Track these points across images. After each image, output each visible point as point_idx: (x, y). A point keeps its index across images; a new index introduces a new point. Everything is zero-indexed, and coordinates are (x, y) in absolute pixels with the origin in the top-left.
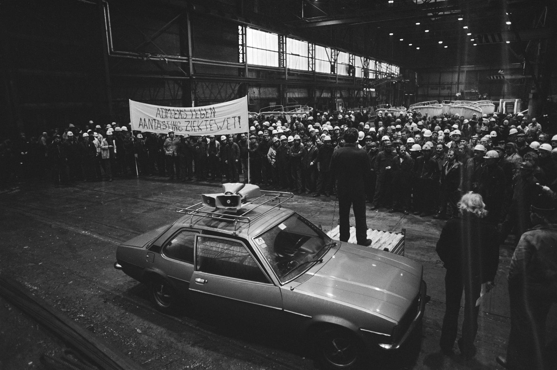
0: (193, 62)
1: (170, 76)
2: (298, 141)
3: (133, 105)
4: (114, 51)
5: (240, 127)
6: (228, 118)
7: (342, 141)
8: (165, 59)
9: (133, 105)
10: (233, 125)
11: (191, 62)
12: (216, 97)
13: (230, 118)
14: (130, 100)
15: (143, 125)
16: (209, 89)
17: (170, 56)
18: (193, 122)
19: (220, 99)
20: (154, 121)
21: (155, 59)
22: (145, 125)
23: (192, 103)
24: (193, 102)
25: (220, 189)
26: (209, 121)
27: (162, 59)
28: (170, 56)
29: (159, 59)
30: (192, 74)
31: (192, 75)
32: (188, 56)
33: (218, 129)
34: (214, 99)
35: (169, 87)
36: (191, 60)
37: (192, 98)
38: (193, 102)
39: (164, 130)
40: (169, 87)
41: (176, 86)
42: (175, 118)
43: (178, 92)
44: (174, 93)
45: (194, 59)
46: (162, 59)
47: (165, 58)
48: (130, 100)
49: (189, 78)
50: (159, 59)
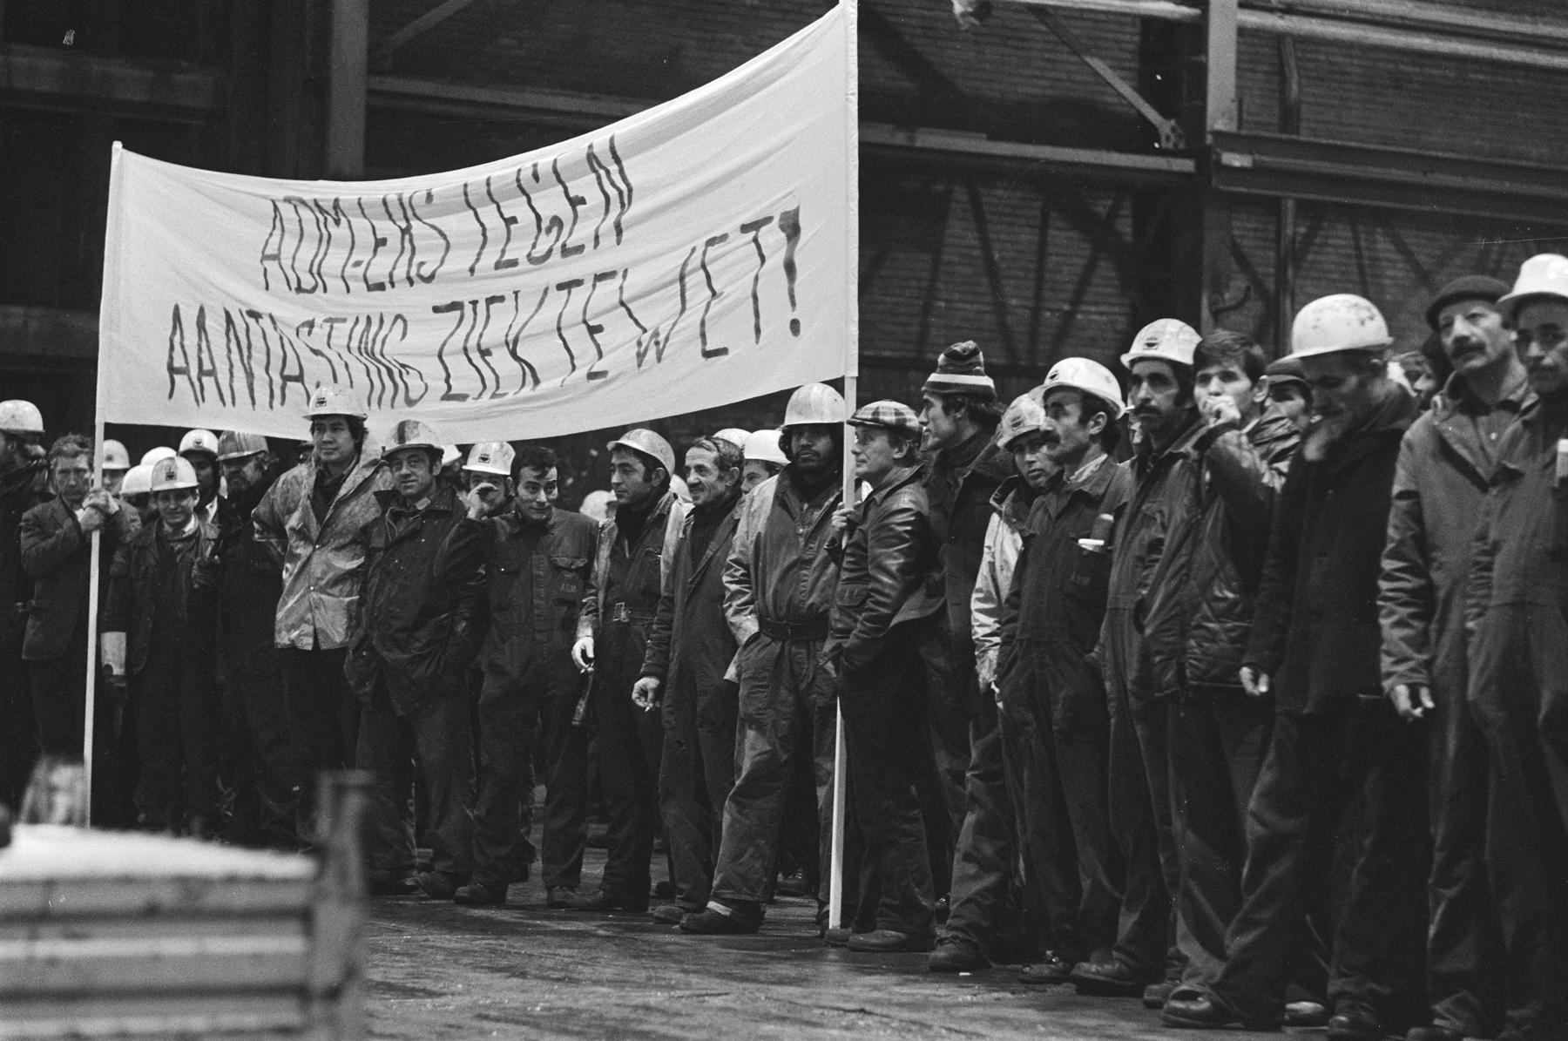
1: (993, 137)
5: (795, 326)
6: (711, 242)
7: (1472, 318)
10: (672, 283)
13: (724, 237)
15: (194, 372)
18: (481, 307)
20: (251, 321)
22: (202, 372)
26: (588, 284)
30: (1220, 125)
31: (1218, 134)
35: (986, 244)
40: (986, 244)
43: (1077, 300)
44: (1036, 312)
49: (1187, 165)
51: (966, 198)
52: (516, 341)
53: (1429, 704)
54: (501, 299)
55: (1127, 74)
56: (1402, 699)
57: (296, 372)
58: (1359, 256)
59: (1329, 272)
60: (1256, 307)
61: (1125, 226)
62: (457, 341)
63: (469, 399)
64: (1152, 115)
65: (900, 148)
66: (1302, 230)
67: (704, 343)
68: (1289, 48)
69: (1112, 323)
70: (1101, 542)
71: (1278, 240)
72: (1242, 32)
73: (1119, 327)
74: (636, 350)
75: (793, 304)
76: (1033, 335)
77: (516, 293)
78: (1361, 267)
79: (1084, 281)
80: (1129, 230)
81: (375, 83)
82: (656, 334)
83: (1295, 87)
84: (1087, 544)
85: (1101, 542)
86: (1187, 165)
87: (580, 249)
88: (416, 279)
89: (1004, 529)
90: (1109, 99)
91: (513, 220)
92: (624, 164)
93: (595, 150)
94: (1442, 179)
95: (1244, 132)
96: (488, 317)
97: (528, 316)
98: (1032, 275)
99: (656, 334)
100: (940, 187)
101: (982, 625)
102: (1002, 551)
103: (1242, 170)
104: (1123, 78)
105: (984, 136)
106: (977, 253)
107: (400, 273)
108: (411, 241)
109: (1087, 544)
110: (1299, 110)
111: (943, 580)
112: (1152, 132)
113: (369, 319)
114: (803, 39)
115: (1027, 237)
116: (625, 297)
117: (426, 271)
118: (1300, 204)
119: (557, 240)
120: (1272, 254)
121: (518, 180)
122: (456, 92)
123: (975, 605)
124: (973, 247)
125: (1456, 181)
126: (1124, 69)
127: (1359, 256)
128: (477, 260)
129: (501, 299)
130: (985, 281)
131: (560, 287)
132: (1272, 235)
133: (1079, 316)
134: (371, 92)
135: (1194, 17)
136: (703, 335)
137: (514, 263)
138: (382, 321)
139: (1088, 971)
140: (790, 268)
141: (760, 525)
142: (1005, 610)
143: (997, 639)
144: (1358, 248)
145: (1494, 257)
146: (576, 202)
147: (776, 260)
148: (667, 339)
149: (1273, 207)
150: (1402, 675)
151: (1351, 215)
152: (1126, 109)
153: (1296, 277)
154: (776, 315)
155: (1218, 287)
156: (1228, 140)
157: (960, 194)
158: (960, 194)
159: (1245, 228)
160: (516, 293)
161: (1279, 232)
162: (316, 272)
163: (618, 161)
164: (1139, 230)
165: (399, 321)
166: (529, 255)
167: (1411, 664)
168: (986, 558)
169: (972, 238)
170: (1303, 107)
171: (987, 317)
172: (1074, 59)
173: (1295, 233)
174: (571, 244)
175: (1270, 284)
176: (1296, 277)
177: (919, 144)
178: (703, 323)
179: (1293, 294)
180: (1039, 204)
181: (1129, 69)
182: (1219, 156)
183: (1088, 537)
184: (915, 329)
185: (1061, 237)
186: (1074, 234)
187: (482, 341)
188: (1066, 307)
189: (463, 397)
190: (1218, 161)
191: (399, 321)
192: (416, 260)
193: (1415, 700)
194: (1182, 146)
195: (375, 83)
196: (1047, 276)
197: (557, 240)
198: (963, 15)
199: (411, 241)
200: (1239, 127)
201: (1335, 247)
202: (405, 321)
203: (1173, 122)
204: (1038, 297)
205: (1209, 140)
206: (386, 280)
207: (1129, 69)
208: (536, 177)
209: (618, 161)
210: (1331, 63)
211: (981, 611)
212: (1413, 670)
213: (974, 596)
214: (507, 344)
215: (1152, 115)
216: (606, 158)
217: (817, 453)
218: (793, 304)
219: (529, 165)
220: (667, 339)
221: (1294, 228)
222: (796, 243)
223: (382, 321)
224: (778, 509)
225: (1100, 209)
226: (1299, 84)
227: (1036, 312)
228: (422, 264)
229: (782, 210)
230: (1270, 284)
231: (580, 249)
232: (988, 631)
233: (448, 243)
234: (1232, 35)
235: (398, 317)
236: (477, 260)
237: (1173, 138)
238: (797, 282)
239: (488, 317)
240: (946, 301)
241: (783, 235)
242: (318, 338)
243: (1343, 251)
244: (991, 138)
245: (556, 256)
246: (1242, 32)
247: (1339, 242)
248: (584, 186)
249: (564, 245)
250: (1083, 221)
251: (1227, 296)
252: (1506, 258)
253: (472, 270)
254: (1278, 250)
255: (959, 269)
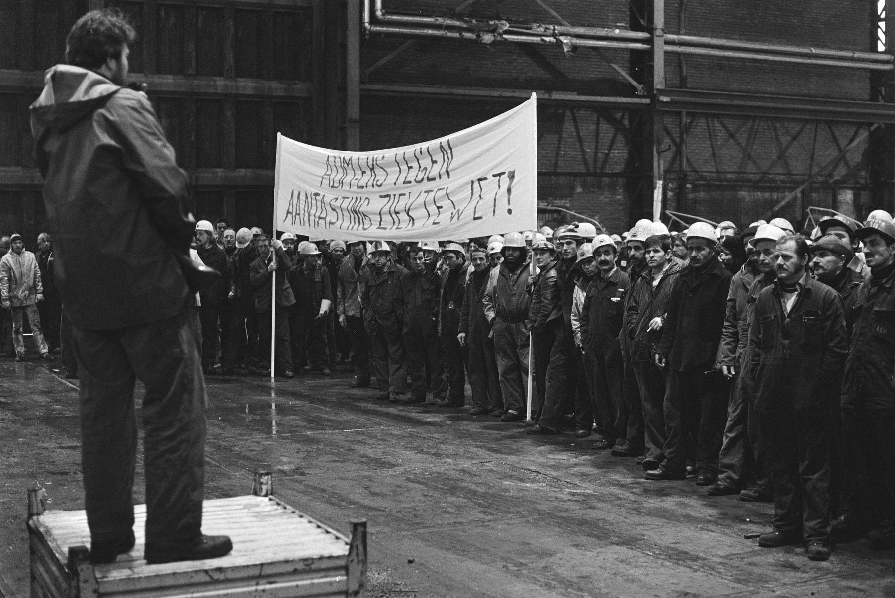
0: (669, 48)
2: (637, 248)
3: (286, 144)
4: (383, 15)
5: (510, 211)
8: (562, 38)
9: (286, 144)
11: (660, 50)
12: (765, 174)
14: (279, 134)
15: (294, 214)
16: (739, 144)
17: (581, 30)
18: (397, 197)
19: (783, 182)
21: (523, 38)
23: (652, 188)
24: (660, 184)
25: (766, 540)
27: (548, 39)
28: (581, 30)
29: (538, 39)
30: (659, 87)
31: (658, 90)
32: (651, 29)
33: (452, 218)
34: (759, 181)
36: (659, 44)
37: (656, 171)
38: (660, 184)
39: (331, 226)
41: (607, 131)
42: (358, 187)
43: (610, 148)
44: (596, 154)
45: (671, 37)
46: (548, 39)
47: (562, 34)
48: (279, 134)
49: (648, 101)
50: (538, 39)
51: (570, 115)
52: (409, 210)
53: (734, 373)
54: (404, 195)
55: (626, 68)
56: (726, 372)
57: (324, 216)
58: (709, 129)
59: (697, 135)
60: (673, 149)
61: (626, 122)
62: (386, 209)
63: (387, 229)
64: (635, 83)
65: (547, 99)
66: (688, 121)
67: (475, 214)
68: (682, 57)
69: (622, 156)
70: (619, 299)
71: (680, 124)
72: (666, 53)
73: (625, 157)
74: (451, 215)
75: (509, 203)
76: (595, 161)
77: (410, 193)
78: (709, 132)
79: (613, 142)
80: (627, 123)
81: (363, 86)
82: (459, 211)
83: (685, 71)
84: (614, 299)
85: (619, 299)
86: (648, 101)
87: (434, 179)
88: (375, 186)
89: (580, 292)
90: (620, 78)
91: (411, 167)
92: (453, 150)
93: (442, 144)
94: (737, 102)
95: (667, 89)
96: (399, 201)
97: (414, 199)
98: (594, 141)
99: (459, 211)
100: (561, 111)
101: (574, 325)
102: (580, 299)
103: (667, 102)
104: (624, 70)
105: (576, 93)
106: (574, 134)
107: (370, 183)
108: (374, 172)
109: (614, 299)
110: (686, 78)
111: (562, 304)
112: (636, 89)
113: (356, 198)
114: (517, 111)
115: (592, 127)
116: (448, 192)
117: (379, 183)
118: (687, 113)
119: (425, 175)
120: (678, 129)
121: (415, 153)
122: (391, 88)
123: (572, 318)
124: (573, 132)
125: (742, 103)
126: (624, 67)
127: (709, 129)
128: (397, 180)
129: (404, 195)
130: (578, 144)
131: (425, 192)
132: (678, 123)
133: (611, 154)
134: (361, 90)
135: (649, 49)
136: (475, 212)
137: (410, 182)
138: (361, 199)
139: (618, 449)
140: (509, 191)
141: (495, 283)
142: (583, 318)
143: (579, 329)
144: (708, 126)
145: (756, 127)
146: (434, 162)
147: (504, 187)
148: (462, 212)
149: (679, 114)
150: (726, 362)
151: (706, 116)
152: (625, 81)
153: (686, 137)
154: (502, 206)
155: (659, 143)
156: (662, 92)
157: (568, 113)
158: (568, 113)
159: (668, 121)
160: (410, 193)
161: (680, 122)
162: (341, 183)
163: (451, 149)
164: (631, 122)
165: (367, 200)
166: (415, 180)
167: (730, 358)
168: (574, 301)
169: (573, 129)
170: (688, 77)
171: (579, 156)
172: (606, 64)
173: (686, 122)
174: (430, 176)
175: (678, 140)
176: (686, 137)
177: (553, 98)
178: (475, 208)
179: (686, 144)
180: (596, 116)
181: (627, 67)
182: (659, 98)
183: (614, 297)
184: (553, 161)
185: (604, 126)
186: (608, 126)
187: (396, 209)
188: (606, 151)
189: (385, 228)
190: (658, 100)
191: (367, 200)
192: (376, 179)
193: (730, 372)
194: (645, 94)
195: (363, 86)
196: (599, 141)
197: (425, 175)
198: (568, 52)
199: (374, 172)
200: (666, 87)
201: (700, 126)
202: (369, 200)
203: (642, 86)
204: (596, 148)
205: (655, 92)
206: (365, 185)
207: (627, 67)
208: (421, 152)
209: (451, 149)
210: (698, 62)
211: (574, 320)
212: (730, 360)
213: (572, 314)
214: (405, 210)
215: (635, 83)
216: (447, 148)
217: (514, 257)
218: (509, 203)
219: (419, 148)
220: (462, 212)
221: (685, 120)
222: (512, 182)
223: (361, 199)
224: (502, 277)
225: (618, 117)
226: (686, 69)
227: (596, 154)
228: (378, 181)
229: (508, 170)
230: (678, 140)
231: (434, 179)
232: (577, 326)
233: (387, 174)
234: (662, 54)
235: (367, 198)
236: (397, 180)
237: (642, 91)
238: (511, 196)
239: (399, 201)
240: (564, 151)
241: (508, 179)
242: (338, 203)
243: (703, 127)
244: (579, 94)
245: (425, 181)
246: (666, 52)
247: (701, 124)
248: (438, 157)
249: (428, 178)
250: (611, 121)
251: (663, 146)
252: (760, 127)
253: (395, 184)
254: (680, 128)
255: (569, 140)
